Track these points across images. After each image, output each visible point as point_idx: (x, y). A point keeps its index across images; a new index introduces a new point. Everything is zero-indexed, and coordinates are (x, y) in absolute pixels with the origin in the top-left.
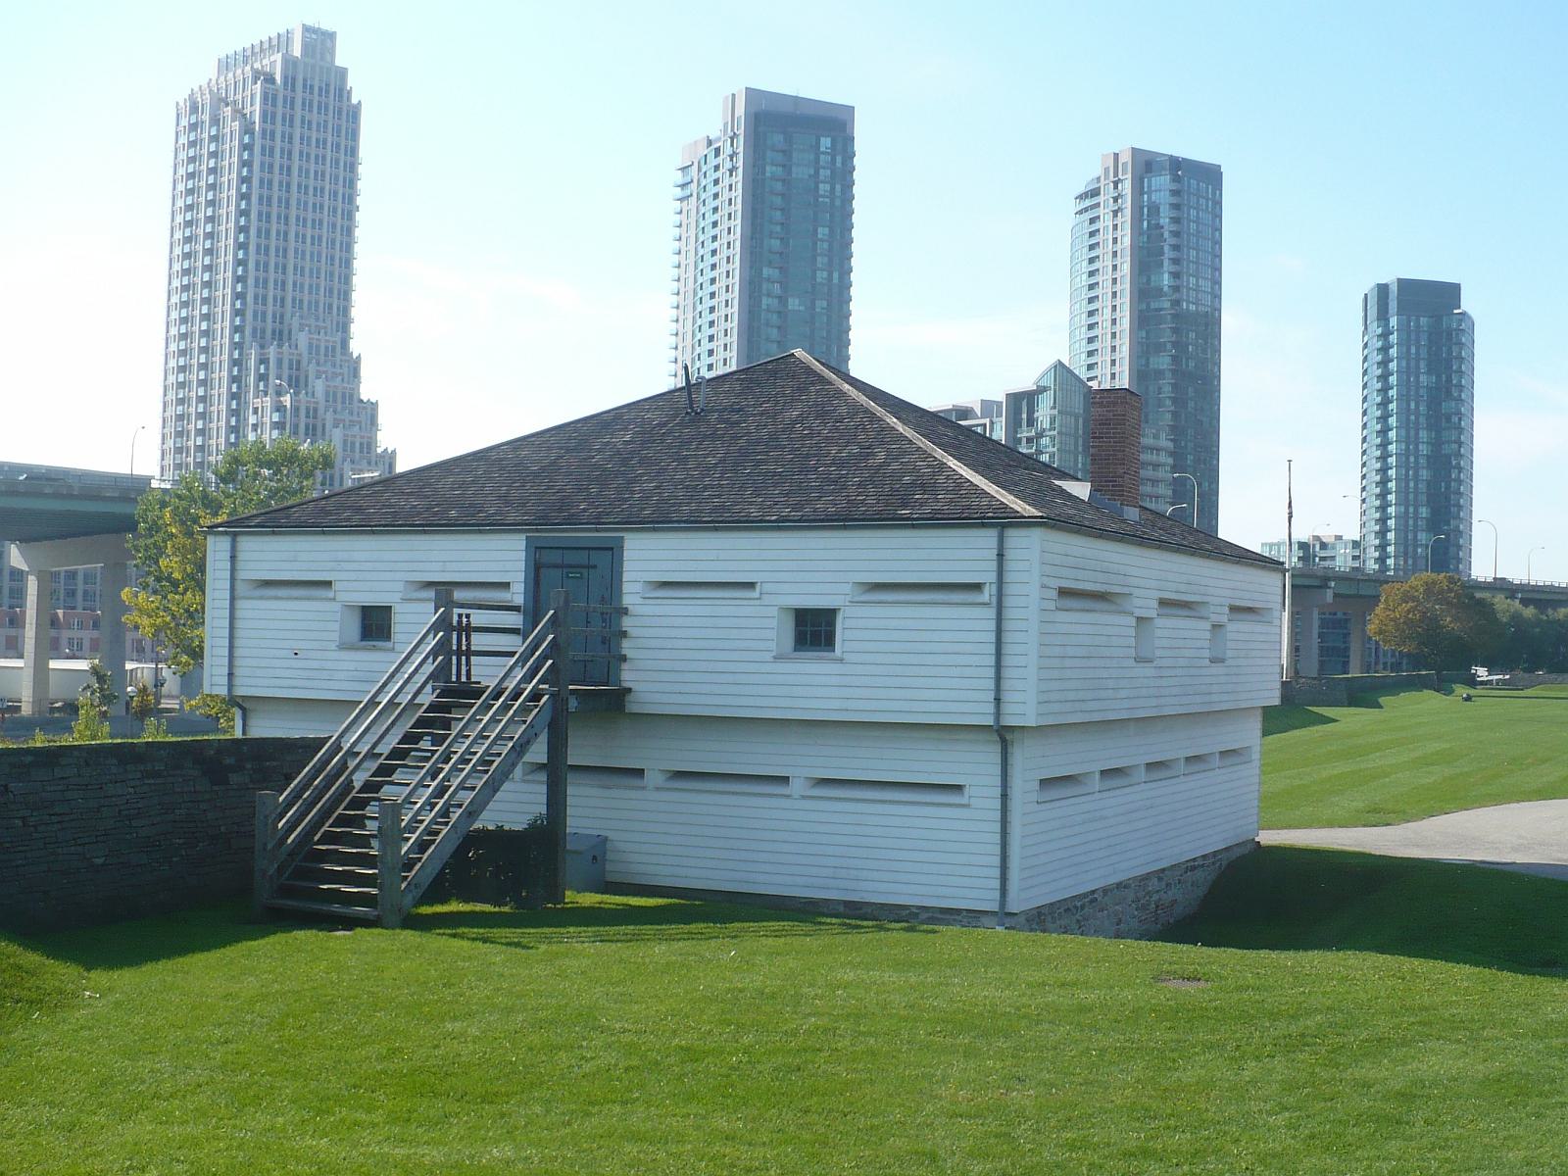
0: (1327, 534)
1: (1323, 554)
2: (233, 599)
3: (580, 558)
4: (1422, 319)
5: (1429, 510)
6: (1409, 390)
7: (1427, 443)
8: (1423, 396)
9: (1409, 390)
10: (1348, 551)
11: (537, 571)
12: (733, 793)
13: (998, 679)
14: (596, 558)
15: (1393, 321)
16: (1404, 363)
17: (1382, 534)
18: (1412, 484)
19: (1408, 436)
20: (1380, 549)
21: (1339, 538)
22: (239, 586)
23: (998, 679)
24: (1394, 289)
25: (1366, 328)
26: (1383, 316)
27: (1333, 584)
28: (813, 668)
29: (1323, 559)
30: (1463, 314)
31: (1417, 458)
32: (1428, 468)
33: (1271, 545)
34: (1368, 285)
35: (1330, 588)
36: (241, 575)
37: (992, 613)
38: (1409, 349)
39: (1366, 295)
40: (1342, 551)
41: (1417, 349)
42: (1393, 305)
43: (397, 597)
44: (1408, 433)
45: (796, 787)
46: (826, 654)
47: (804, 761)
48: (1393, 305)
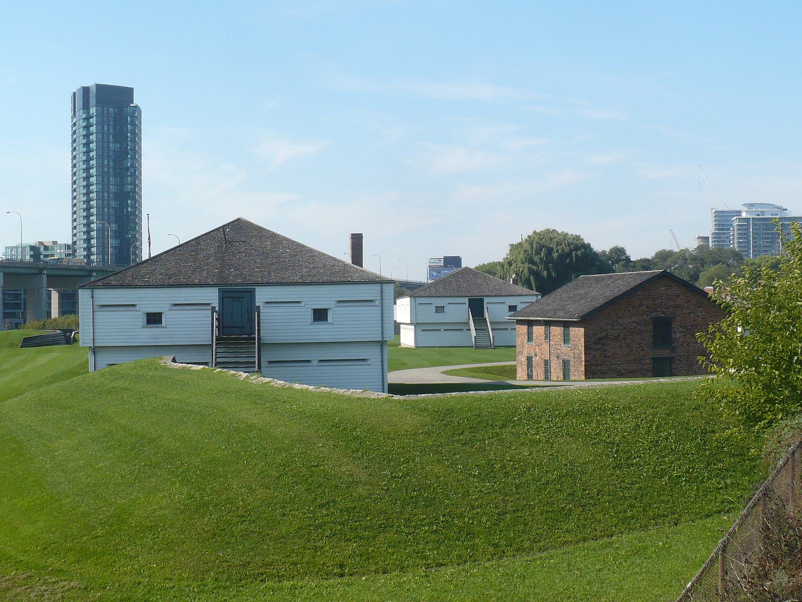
0: (47, 240)
1: (46, 253)
2: (93, 311)
3: (239, 295)
4: (110, 109)
5: (116, 225)
6: (103, 152)
7: (114, 185)
8: (112, 157)
9: (103, 152)
10: (62, 251)
11: (222, 299)
12: (301, 366)
13: (382, 327)
14: (244, 295)
15: (93, 110)
16: (100, 136)
17: (88, 240)
18: (106, 210)
19: (103, 180)
20: (87, 249)
21: (55, 243)
22: (95, 306)
23: (382, 327)
24: (93, 90)
25: (75, 113)
26: (86, 106)
27: (95, 274)
28: (320, 326)
29: (46, 256)
30: (136, 107)
31: (108, 194)
32: (115, 199)
33: (12, 248)
34: (76, 86)
35: (93, 276)
36: (96, 303)
37: (380, 308)
38: (103, 128)
39: (74, 93)
40: (59, 251)
41: (108, 128)
42: (93, 101)
43: (167, 309)
44: (103, 178)
45: (315, 363)
46: (159, 325)
47: (315, 355)
48: (93, 101)
